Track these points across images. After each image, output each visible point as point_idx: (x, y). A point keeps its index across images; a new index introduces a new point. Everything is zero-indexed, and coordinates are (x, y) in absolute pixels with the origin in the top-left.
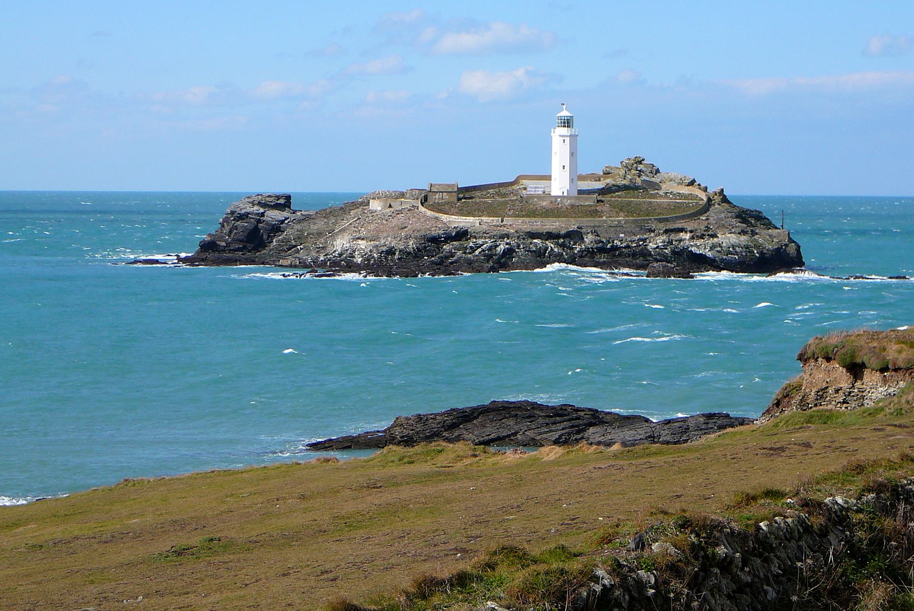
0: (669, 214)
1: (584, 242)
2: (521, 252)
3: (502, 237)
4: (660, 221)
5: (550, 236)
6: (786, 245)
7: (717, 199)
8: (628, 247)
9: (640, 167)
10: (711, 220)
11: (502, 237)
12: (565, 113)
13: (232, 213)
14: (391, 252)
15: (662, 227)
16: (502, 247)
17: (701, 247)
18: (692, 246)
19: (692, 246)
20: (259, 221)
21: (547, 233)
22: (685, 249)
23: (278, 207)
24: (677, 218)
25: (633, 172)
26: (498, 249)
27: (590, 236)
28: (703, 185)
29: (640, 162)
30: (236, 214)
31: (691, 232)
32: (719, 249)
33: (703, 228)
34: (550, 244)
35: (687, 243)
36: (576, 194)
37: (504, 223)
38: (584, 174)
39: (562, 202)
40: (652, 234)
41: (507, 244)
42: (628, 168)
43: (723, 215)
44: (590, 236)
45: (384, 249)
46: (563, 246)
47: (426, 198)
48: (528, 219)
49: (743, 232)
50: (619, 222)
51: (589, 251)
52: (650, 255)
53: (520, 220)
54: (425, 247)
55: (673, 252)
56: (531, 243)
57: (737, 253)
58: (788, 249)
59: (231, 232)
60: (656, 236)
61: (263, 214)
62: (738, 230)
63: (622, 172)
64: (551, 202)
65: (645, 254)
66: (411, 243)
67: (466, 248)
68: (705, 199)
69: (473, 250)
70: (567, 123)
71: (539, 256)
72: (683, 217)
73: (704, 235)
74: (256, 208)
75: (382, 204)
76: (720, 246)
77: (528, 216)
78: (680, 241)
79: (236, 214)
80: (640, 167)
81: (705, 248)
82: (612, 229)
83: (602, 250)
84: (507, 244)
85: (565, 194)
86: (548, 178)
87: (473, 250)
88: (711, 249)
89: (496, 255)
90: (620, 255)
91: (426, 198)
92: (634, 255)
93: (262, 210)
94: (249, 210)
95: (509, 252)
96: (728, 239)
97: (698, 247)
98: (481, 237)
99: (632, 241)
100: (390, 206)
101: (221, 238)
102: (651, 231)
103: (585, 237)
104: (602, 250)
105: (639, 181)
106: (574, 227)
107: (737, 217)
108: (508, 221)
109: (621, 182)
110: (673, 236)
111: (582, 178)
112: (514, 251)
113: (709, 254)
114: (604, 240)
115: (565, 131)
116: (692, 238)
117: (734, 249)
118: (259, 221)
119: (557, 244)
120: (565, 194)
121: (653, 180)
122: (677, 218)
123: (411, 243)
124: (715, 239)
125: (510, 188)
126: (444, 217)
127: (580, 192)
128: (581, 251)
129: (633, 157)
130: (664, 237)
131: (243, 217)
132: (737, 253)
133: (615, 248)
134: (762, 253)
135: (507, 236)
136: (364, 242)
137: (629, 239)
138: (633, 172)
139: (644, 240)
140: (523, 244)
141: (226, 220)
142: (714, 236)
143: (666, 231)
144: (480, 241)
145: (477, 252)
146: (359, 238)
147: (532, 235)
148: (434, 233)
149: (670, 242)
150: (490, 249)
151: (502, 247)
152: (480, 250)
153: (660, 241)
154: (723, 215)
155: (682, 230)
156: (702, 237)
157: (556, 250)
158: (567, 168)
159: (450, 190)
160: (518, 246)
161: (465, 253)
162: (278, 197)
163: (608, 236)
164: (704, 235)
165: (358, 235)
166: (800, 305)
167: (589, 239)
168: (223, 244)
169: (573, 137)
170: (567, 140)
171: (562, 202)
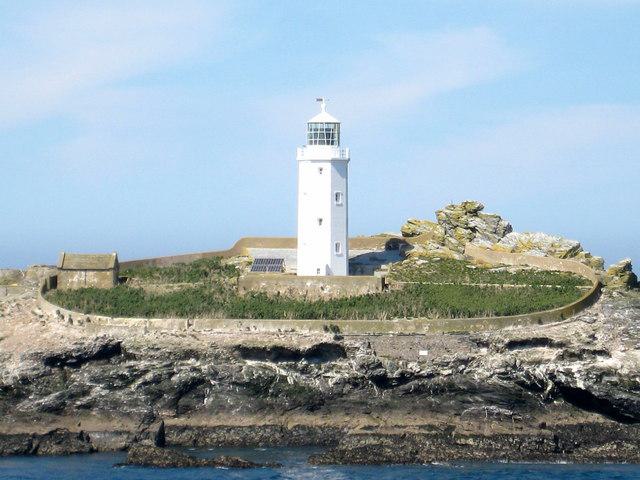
5: (280, 353)
7: (618, 283)
9: (474, 222)
12: (324, 117)
25: (462, 231)
28: (595, 258)
29: (475, 213)
36: (342, 270)
38: (368, 235)
41: (194, 369)
42: (450, 223)
47: (54, 281)
63: (440, 231)
68: (595, 283)
70: (328, 135)
80: (474, 222)
82: (404, 341)
86: (291, 242)
91: (54, 281)
111: (352, 243)
116: (561, 358)
120: (323, 273)
129: (458, 203)
139: (465, 362)
142: (604, 353)
144: (142, 364)
145: (133, 387)
147: (247, 352)
148: (57, 350)
150: (157, 380)
152: (140, 381)
158: (327, 222)
165: (412, 339)
169: (341, 166)
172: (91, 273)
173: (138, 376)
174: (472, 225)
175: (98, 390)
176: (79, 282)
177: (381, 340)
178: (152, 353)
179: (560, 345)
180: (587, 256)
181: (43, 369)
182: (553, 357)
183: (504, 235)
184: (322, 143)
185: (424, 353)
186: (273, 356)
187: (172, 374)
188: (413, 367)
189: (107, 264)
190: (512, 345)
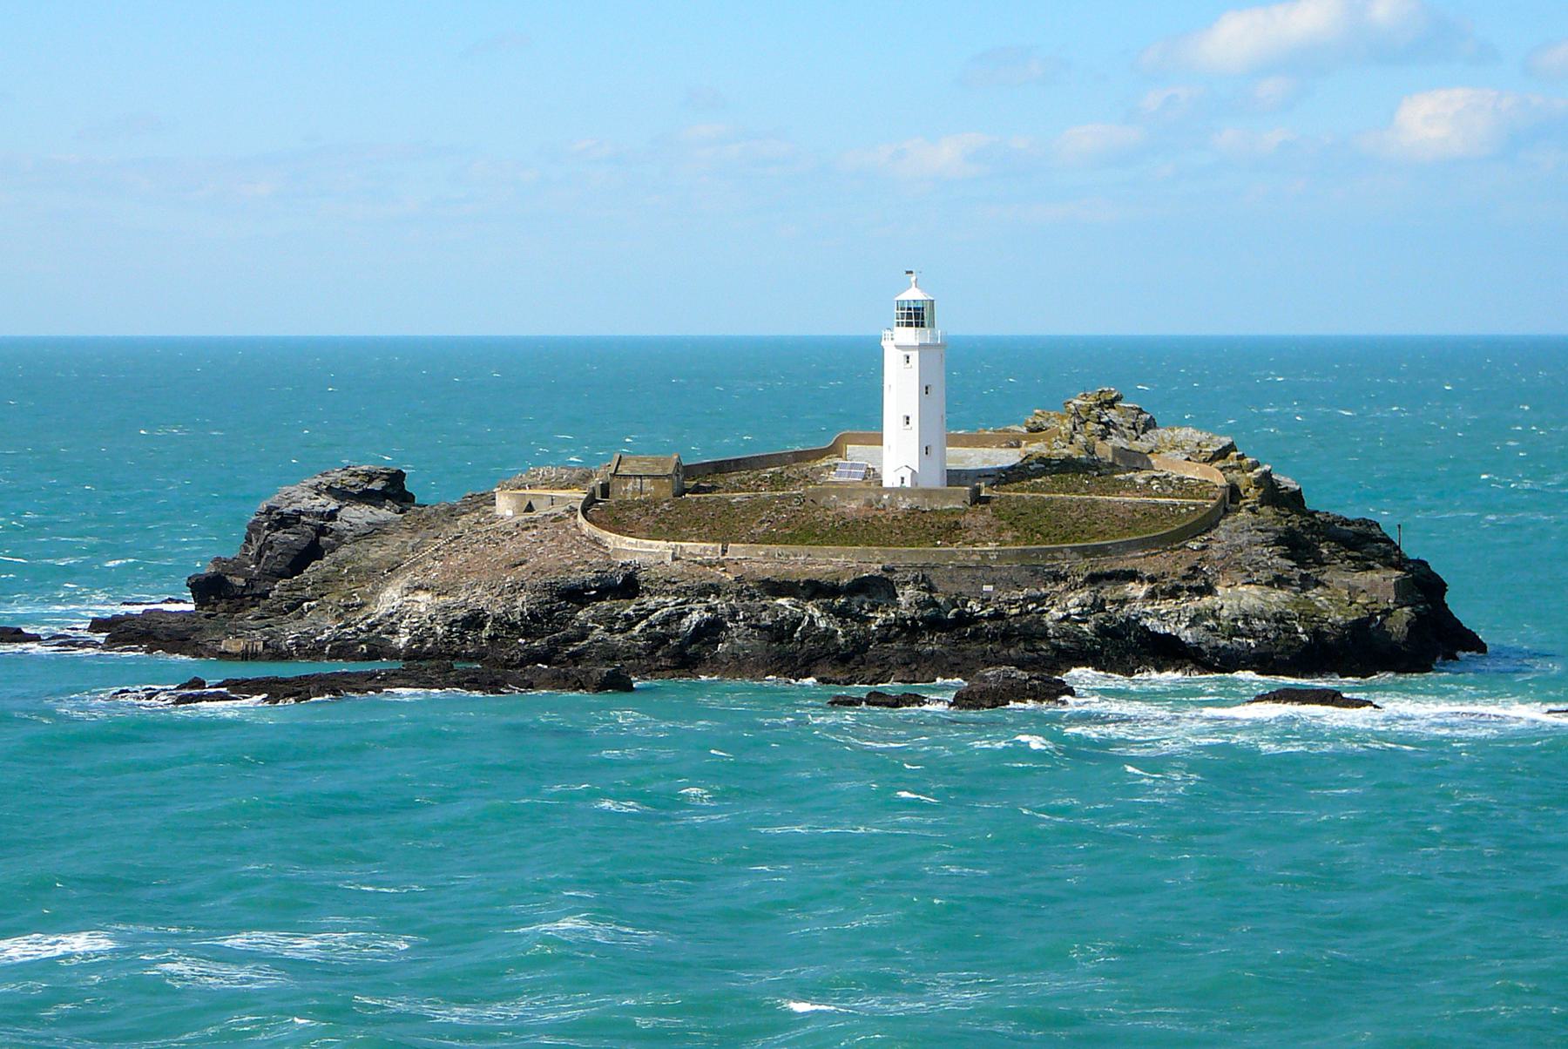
0: (1121, 534)
1: (898, 605)
2: (737, 629)
3: (704, 591)
4: (1084, 552)
5: (815, 589)
6: (1387, 613)
7: (1253, 494)
8: (998, 615)
9: (1112, 415)
10: (1215, 552)
11: (704, 591)
12: (913, 295)
13: (270, 510)
14: (474, 621)
15: (1084, 566)
16: (695, 617)
17: (1170, 619)
18: (1147, 615)
19: (1147, 615)
20: (321, 531)
21: (808, 582)
22: (1131, 623)
23: (367, 497)
24: (1130, 546)
25: (1092, 426)
26: (685, 621)
27: (910, 591)
29: (1111, 404)
30: (274, 516)
31: (1152, 580)
32: (1211, 623)
33: (1182, 570)
34: (812, 609)
35: (1138, 606)
37: (728, 556)
39: (892, 503)
40: (1062, 586)
43: (1245, 538)
44: (910, 591)
45: (460, 614)
46: (842, 613)
48: (776, 549)
49: (1279, 582)
50: (985, 555)
51: (904, 627)
52: (1044, 636)
53: (762, 550)
54: (551, 612)
55: (1101, 630)
56: (765, 608)
57: (1253, 634)
58: (1389, 622)
59: (260, 554)
60: (1069, 589)
61: (332, 516)
62: (1263, 575)
64: (869, 504)
65: (1033, 633)
66: (519, 603)
67: (615, 619)
69: (630, 622)
70: (916, 316)
71: (779, 639)
72: (1143, 544)
73: (1179, 588)
74: (322, 500)
75: (514, 502)
76: (1214, 614)
77: (791, 540)
78: (1123, 602)
79: (274, 516)
80: (1112, 415)
81: (1178, 622)
82: (965, 573)
83: (935, 624)
84: (708, 609)
85: (908, 484)
86: (878, 440)
87: (630, 622)
88: (1193, 622)
89: (677, 635)
90: (975, 636)
92: (1006, 637)
93: (333, 505)
94: (306, 504)
95: (711, 630)
96: (1237, 597)
97: (1161, 618)
98: (659, 592)
99: (1010, 603)
100: (530, 508)
101: (238, 566)
102: (1057, 578)
103: (899, 592)
104: (935, 624)
105: (1105, 450)
106: (875, 569)
107: (1278, 542)
108: (737, 551)
109: (1061, 450)
110: (1108, 592)
112: (722, 626)
113: (1187, 635)
114: (941, 600)
115: (909, 335)
116: (1152, 595)
117: (1246, 623)
118: (321, 531)
119: (828, 609)
120: (908, 484)
121: (1137, 445)
122: (1130, 546)
123: (519, 603)
124: (1207, 600)
125: (806, 467)
126: (611, 539)
127: (955, 477)
128: (886, 626)
130: (1085, 594)
131: (285, 521)
132: (1253, 634)
133: (964, 619)
134: (1316, 634)
135: (716, 590)
136: (429, 596)
137: (1005, 597)
138: (1092, 426)
139: (1040, 600)
140: (747, 609)
141: (254, 528)
142: (1209, 590)
143: (1094, 579)
144: (651, 603)
146: (419, 588)
147: (777, 588)
148: (574, 579)
149: (1099, 606)
150: (665, 622)
151: (695, 617)
152: (644, 623)
153: (1074, 602)
154: (1245, 538)
155: (1132, 576)
156: (1174, 593)
157: (822, 624)
158: (914, 421)
159: (658, 472)
160: (733, 614)
161: (610, 630)
162: (371, 477)
163: (953, 589)
164: (1179, 588)
166: (874, 835)
167: (907, 596)
168: (240, 581)
170: (915, 355)
171: (892, 503)
172: (646, 481)
173: (645, 617)
174: (1105, 419)
175: (599, 632)
176: (634, 491)
177: (938, 572)
178: (668, 587)
179: (1152, 580)
180: (1240, 457)
181: (956, 501)
182: (1142, 594)
183: (1144, 432)
184: (909, 325)
185: (989, 588)
186: (808, 592)
187: (683, 615)
188: (974, 606)
189: (665, 469)
190: (1094, 579)
